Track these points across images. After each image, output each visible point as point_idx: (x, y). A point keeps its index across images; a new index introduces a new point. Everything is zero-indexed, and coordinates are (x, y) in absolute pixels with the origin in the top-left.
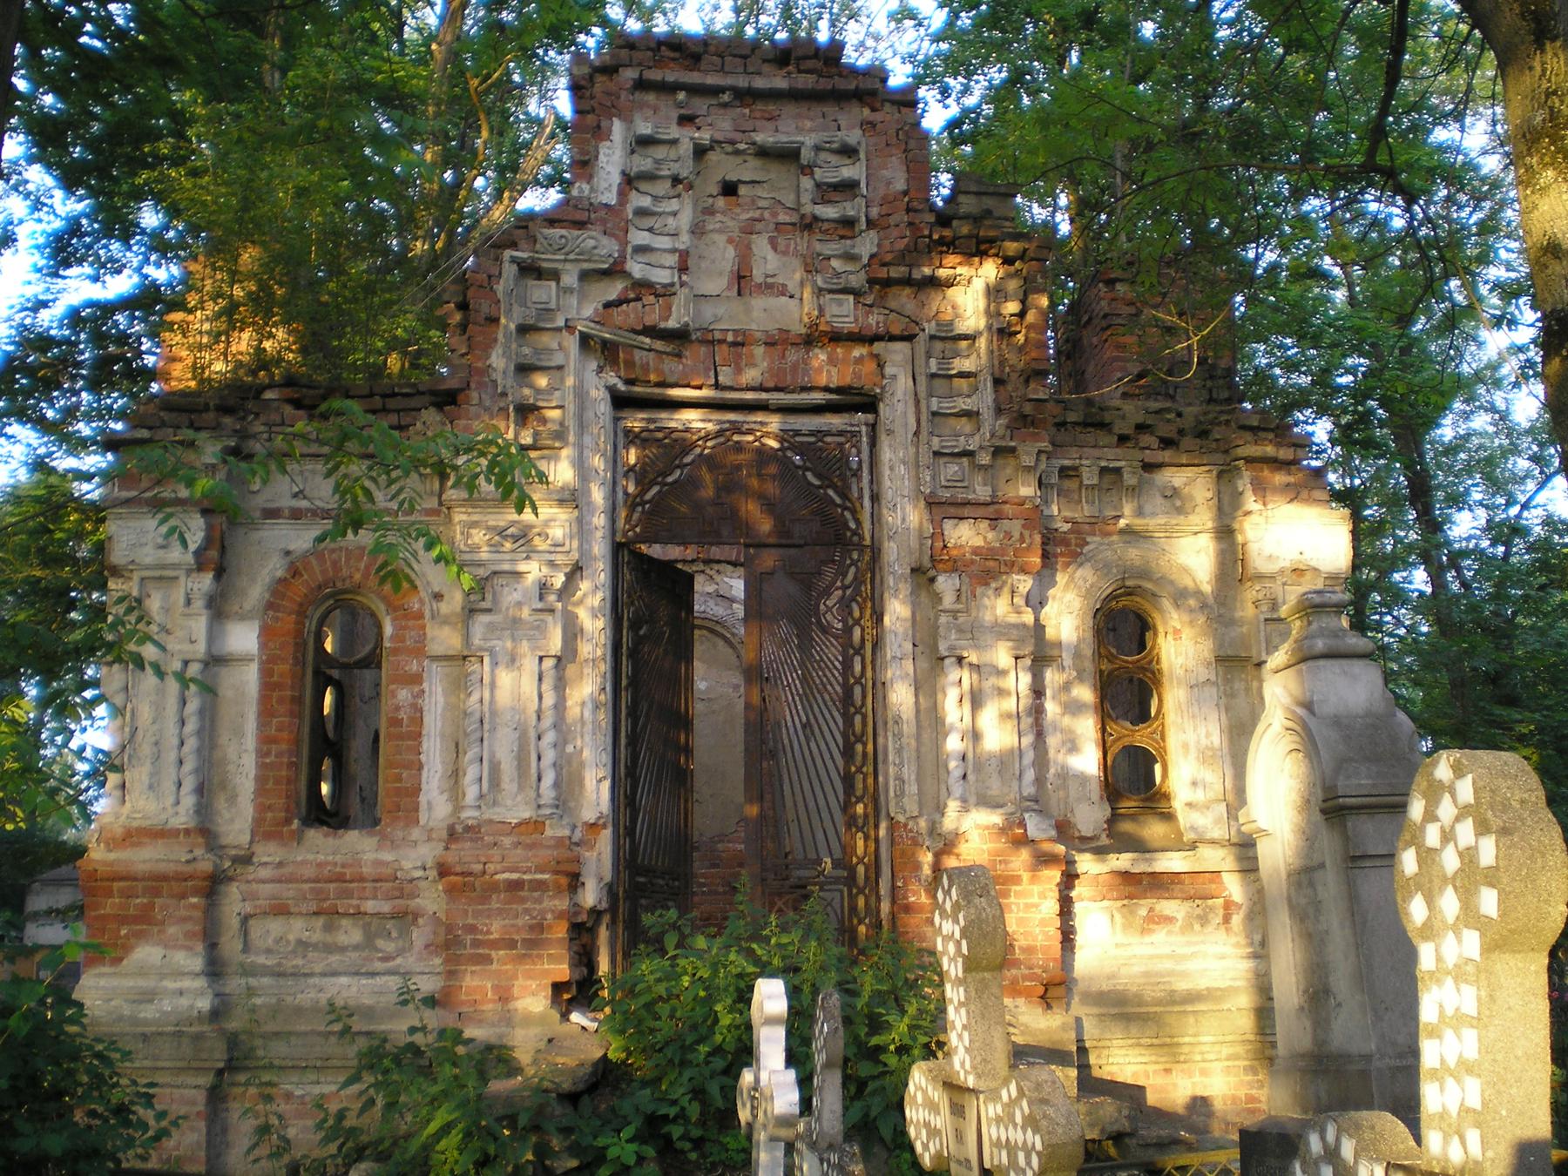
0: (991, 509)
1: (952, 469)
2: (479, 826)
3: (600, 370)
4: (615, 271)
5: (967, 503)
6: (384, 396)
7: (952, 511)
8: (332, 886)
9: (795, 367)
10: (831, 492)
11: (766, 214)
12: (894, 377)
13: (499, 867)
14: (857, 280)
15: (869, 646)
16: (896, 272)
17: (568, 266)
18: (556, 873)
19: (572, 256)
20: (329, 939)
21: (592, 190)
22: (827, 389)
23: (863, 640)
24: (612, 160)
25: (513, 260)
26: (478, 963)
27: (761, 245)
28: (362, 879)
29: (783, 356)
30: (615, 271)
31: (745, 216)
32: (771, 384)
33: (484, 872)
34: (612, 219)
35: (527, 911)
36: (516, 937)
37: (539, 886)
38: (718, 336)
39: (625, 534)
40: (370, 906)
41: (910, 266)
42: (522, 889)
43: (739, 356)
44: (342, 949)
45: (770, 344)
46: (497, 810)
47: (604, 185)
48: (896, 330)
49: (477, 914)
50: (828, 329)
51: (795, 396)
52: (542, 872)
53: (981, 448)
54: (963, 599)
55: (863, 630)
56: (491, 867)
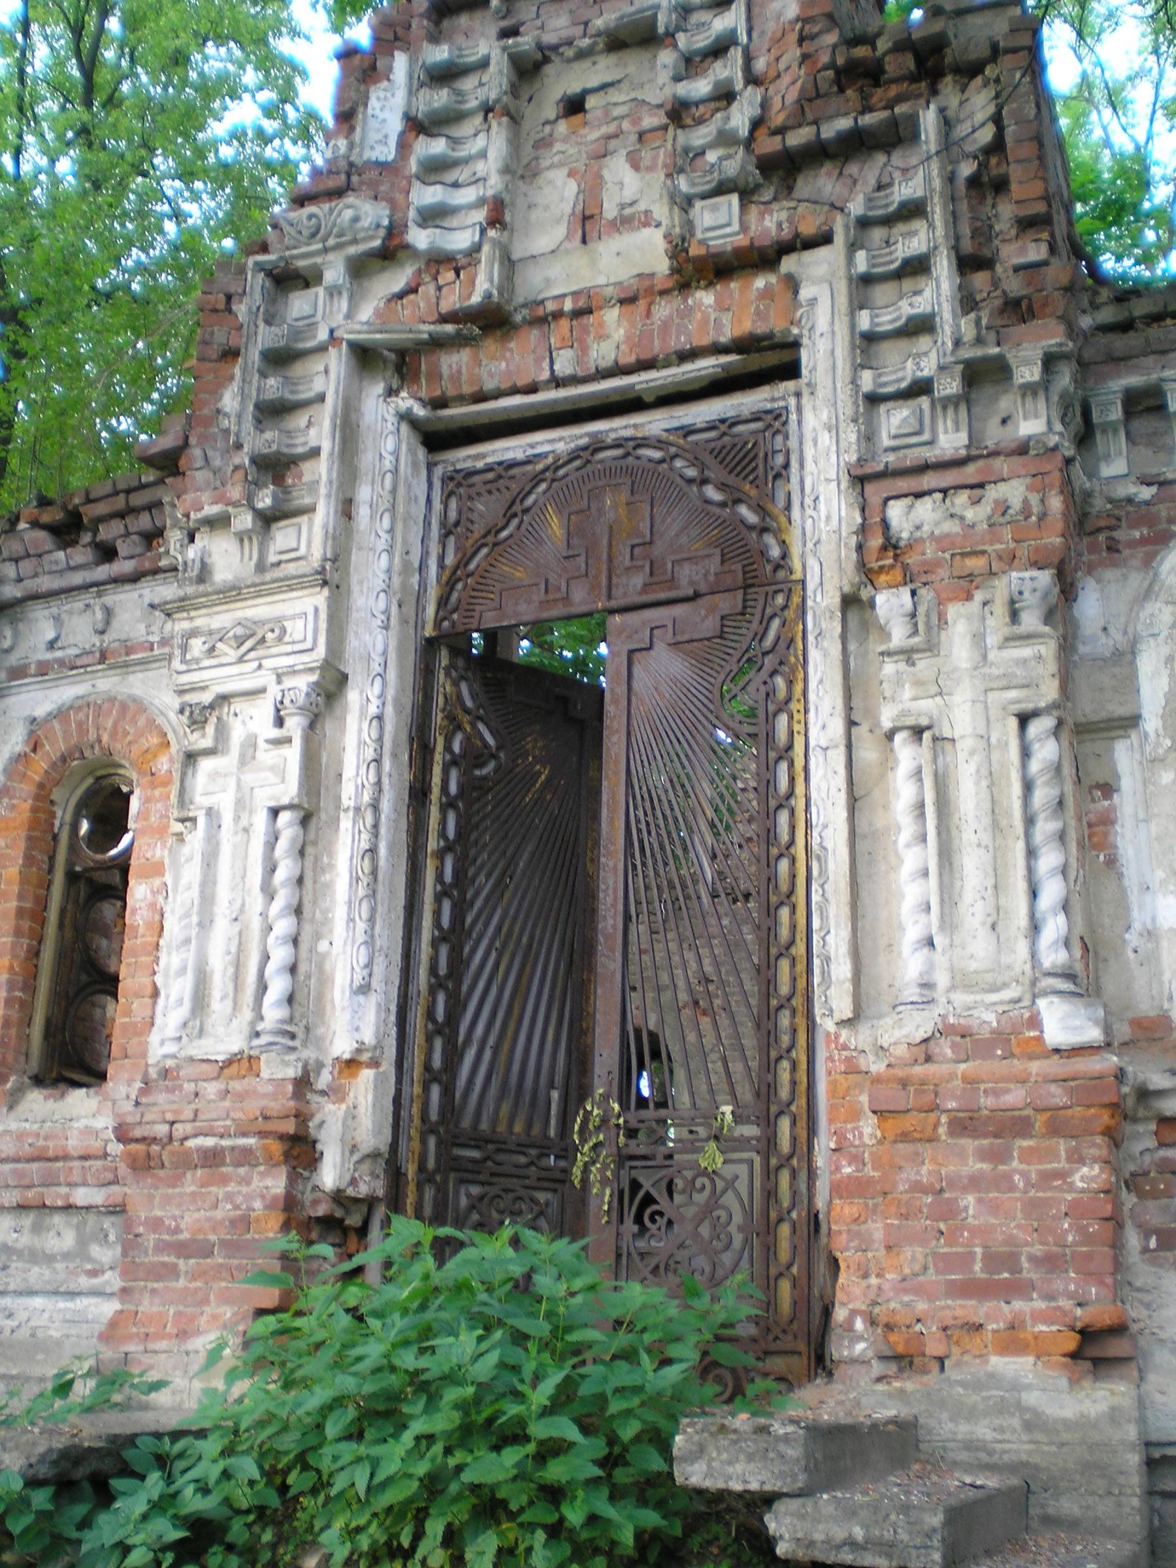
0: (971, 469)
1: (895, 420)
2: (178, 1068)
4: (391, 251)
5: (924, 468)
6: (128, 492)
7: (902, 484)
8: (35, 1166)
9: (666, 326)
11: (626, 125)
12: (813, 302)
13: (189, 1128)
14: (734, 164)
16: (797, 138)
17: (331, 257)
18: (262, 1134)
19: (331, 242)
20: (37, 1243)
21: (351, 146)
22: (718, 349)
23: (791, 734)
24: (387, 109)
25: (260, 267)
26: (159, 1278)
27: (618, 170)
28: (66, 1157)
29: (648, 314)
30: (391, 251)
31: (595, 135)
32: (629, 359)
33: (171, 1138)
34: (381, 178)
35: (229, 1197)
36: (213, 1238)
37: (245, 1157)
38: (551, 306)
39: (438, 623)
40: (82, 1196)
41: (816, 122)
42: (223, 1163)
43: (585, 330)
44: (50, 1259)
45: (628, 301)
46: (203, 1042)
47: (373, 136)
48: (808, 228)
49: (167, 1200)
50: (702, 251)
51: (673, 370)
52: (245, 1134)
53: (941, 368)
55: (791, 717)
56: (179, 1130)
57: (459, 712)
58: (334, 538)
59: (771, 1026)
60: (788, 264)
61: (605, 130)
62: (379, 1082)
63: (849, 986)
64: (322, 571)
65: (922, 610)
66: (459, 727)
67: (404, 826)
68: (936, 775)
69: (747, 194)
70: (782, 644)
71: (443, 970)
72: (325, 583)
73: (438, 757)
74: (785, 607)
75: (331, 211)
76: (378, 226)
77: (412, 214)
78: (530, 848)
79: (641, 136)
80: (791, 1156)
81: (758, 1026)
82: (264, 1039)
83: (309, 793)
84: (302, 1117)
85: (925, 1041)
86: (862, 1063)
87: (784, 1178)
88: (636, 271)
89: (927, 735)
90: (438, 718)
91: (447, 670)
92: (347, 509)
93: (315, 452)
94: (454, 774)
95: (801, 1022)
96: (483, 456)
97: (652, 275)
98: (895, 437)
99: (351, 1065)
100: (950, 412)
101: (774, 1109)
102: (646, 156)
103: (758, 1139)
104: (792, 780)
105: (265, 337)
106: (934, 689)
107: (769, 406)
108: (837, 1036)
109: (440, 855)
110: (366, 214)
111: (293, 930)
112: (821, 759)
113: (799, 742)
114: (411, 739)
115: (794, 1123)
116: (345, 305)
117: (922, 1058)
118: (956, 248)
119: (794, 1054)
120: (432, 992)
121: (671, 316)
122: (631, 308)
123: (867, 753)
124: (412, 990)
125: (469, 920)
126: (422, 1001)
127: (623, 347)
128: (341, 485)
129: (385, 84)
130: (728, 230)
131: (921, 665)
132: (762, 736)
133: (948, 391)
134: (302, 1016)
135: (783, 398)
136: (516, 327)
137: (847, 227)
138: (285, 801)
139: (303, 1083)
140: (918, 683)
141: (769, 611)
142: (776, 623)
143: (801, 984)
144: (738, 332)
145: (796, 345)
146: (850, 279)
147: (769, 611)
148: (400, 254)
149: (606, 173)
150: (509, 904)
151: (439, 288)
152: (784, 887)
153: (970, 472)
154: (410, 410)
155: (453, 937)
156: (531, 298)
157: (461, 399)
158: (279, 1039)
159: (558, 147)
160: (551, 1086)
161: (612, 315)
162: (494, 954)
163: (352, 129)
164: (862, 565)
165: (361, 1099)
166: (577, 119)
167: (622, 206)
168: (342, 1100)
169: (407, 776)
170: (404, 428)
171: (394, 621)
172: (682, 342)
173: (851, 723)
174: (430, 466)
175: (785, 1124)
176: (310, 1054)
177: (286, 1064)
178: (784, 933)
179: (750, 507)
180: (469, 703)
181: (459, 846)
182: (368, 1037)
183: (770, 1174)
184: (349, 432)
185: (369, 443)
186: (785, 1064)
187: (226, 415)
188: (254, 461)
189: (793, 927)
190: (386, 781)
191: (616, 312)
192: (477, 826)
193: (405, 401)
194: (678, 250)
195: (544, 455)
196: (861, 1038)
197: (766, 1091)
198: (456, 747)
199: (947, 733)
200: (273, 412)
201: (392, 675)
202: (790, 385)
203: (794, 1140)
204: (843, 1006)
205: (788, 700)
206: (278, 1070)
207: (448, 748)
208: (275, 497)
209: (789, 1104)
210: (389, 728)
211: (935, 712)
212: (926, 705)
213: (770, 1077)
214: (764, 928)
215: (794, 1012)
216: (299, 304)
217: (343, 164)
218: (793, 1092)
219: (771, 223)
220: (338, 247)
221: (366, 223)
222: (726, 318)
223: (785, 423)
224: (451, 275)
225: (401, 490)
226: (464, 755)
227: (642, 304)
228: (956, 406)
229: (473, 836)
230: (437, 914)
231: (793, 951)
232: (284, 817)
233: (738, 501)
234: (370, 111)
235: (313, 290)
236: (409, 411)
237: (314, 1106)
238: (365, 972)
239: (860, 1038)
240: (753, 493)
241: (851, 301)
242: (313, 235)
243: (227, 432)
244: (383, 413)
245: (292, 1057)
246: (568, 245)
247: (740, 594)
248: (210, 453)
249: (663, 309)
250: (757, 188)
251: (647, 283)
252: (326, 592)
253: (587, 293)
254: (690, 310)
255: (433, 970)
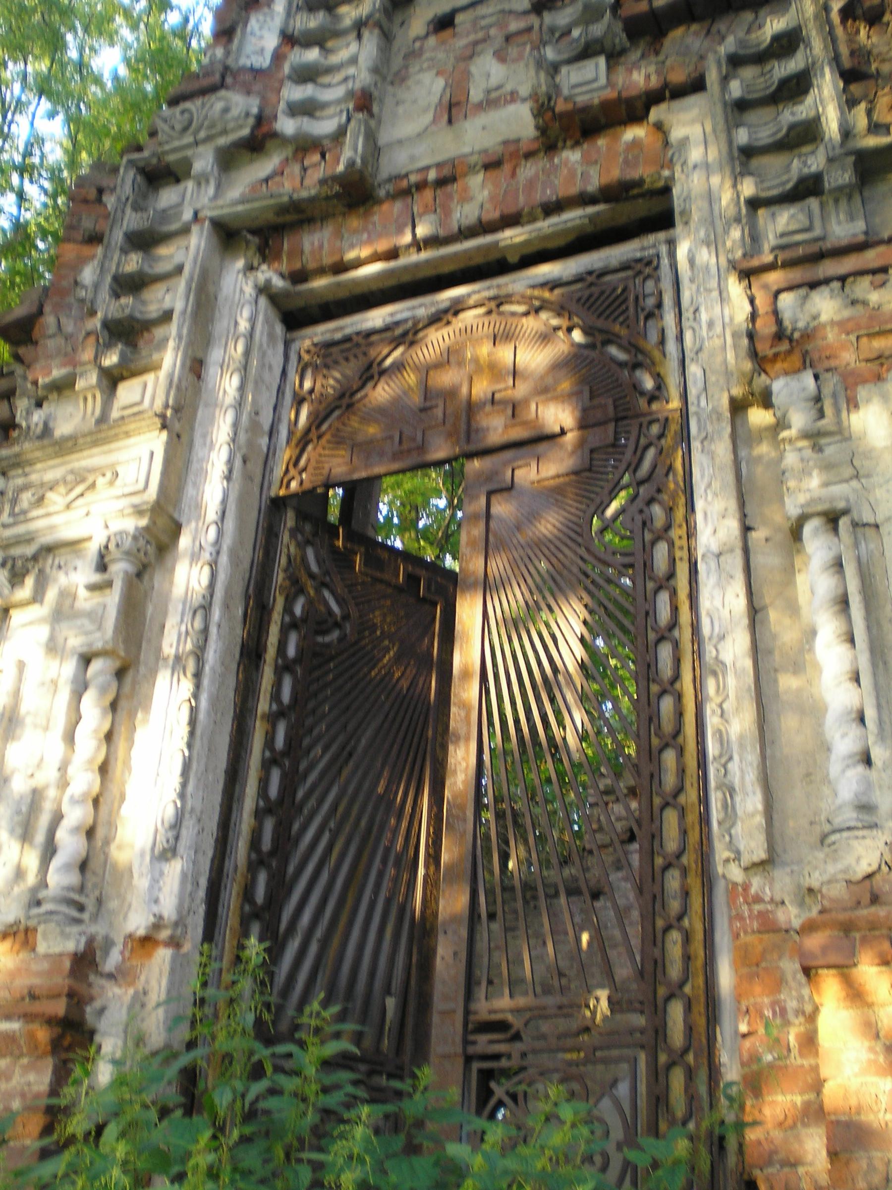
3: (250, 268)
4: (258, 141)
9: (531, 184)
10: (613, 350)
11: (493, 32)
15: (682, 571)
17: (201, 149)
18: (28, 1017)
21: (228, 53)
22: (584, 199)
23: (673, 561)
29: (514, 174)
30: (258, 141)
32: (493, 214)
38: (413, 178)
45: (492, 165)
48: (678, 77)
50: (570, 106)
54: (829, 410)
57: (304, 578)
58: (179, 388)
59: (657, 889)
60: (655, 114)
61: (472, 37)
62: (177, 967)
63: (760, 819)
64: (163, 416)
65: (827, 391)
66: (301, 591)
67: (232, 682)
68: (859, 560)
69: (614, 57)
70: (660, 471)
71: (266, 844)
72: (164, 427)
73: (276, 616)
74: (661, 436)
75: (203, 105)
76: (247, 114)
77: (282, 106)
78: (374, 725)
79: (508, 38)
80: (686, 1051)
81: (640, 891)
82: (47, 907)
83: (127, 641)
84: (77, 999)
85: (869, 876)
86: (781, 916)
87: (677, 1079)
88: (500, 139)
89: (844, 523)
90: (279, 577)
91: (293, 533)
92: (196, 367)
93: (167, 316)
94: (293, 640)
95: (694, 883)
96: (341, 328)
97: (518, 141)
98: (782, 235)
99: (147, 942)
100: (843, 204)
101: (662, 991)
102: (513, 51)
103: (642, 1032)
104: (675, 609)
105: (132, 220)
106: (848, 472)
107: (638, 255)
108: (746, 887)
109: (272, 719)
110: (239, 105)
111: (96, 789)
112: (713, 564)
113: (682, 571)
114: (247, 597)
115: (688, 1008)
116: (211, 191)
117: (866, 898)
118: (836, 59)
119: (686, 922)
120: (253, 867)
121: (537, 175)
122: (493, 174)
123: (767, 560)
124: (229, 866)
125: (300, 794)
126: (239, 877)
127: (487, 206)
128: (190, 344)
129: (266, 10)
130: (595, 85)
131: (829, 451)
132: (639, 566)
133: (840, 182)
134: (95, 886)
135: (654, 246)
136: (379, 202)
137: (719, 63)
138: (99, 645)
139: (85, 962)
140: (828, 467)
141: (643, 441)
142: (651, 453)
143: (694, 837)
144: (605, 180)
145: (666, 191)
146: (725, 104)
147: (643, 441)
148: (269, 144)
149: (473, 69)
150: (348, 782)
151: (305, 169)
152: (668, 726)
153: (872, 257)
154: (268, 282)
155: (281, 809)
156: (395, 172)
157: (321, 271)
158: (64, 909)
159: (427, 55)
160: (388, 991)
161: (476, 181)
162: (326, 837)
163: (230, 40)
164: (754, 354)
165: (154, 983)
166: (448, 32)
167: (489, 92)
168: (132, 983)
169: (239, 632)
170: (263, 301)
171: (236, 474)
172: (549, 195)
173: (746, 529)
174: (287, 344)
175: (676, 1012)
176: (98, 930)
177: (65, 936)
178: (670, 780)
179: (621, 347)
180: (314, 568)
181: (295, 712)
182: (168, 906)
183: (658, 1076)
184: (205, 304)
185: (225, 311)
186: (675, 936)
187: (84, 287)
188: (106, 324)
189: (682, 771)
190: (213, 630)
191: (480, 177)
192: (315, 695)
193: (266, 274)
194: (543, 108)
195: (406, 321)
196: (778, 886)
197: (652, 969)
198: (298, 610)
199: (868, 517)
200: (132, 285)
201: (230, 525)
202: (662, 236)
203: (689, 1029)
204: (754, 847)
205: (668, 527)
206: (58, 943)
207: (288, 609)
208: (123, 356)
209: (681, 985)
210: (222, 577)
211: (852, 498)
212: (838, 490)
213: (657, 952)
214: (646, 772)
215: (685, 872)
216: (167, 197)
217: (219, 68)
218: (686, 970)
219: (640, 77)
220: (209, 139)
221: (235, 112)
222: (594, 172)
223: (657, 268)
224: (316, 157)
225: (255, 354)
226: (305, 619)
227: (507, 168)
228: (850, 197)
229: (311, 705)
230: (264, 783)
231: (682, 799)
232: (96, 665)
233: (607, 342)
234: (249, 29)
235: (181, 186)
236: (268, 284)
237: (95, 991)
238: (171, 834)
239: (779, 885)
240: (624, 332)
241: (727, 121)
242: (185, 129)
243: (82, 301)
244: (241, 286)
245: (75, 929)
246: (434, 128)
247: (611, 427)
248: (63, 320)
249: (528, 170)
250: (623, 52)
251: (512, 148)
252: (164, 435)
253: (452, 163)
254: (556, 168)
255: (255, 843)
